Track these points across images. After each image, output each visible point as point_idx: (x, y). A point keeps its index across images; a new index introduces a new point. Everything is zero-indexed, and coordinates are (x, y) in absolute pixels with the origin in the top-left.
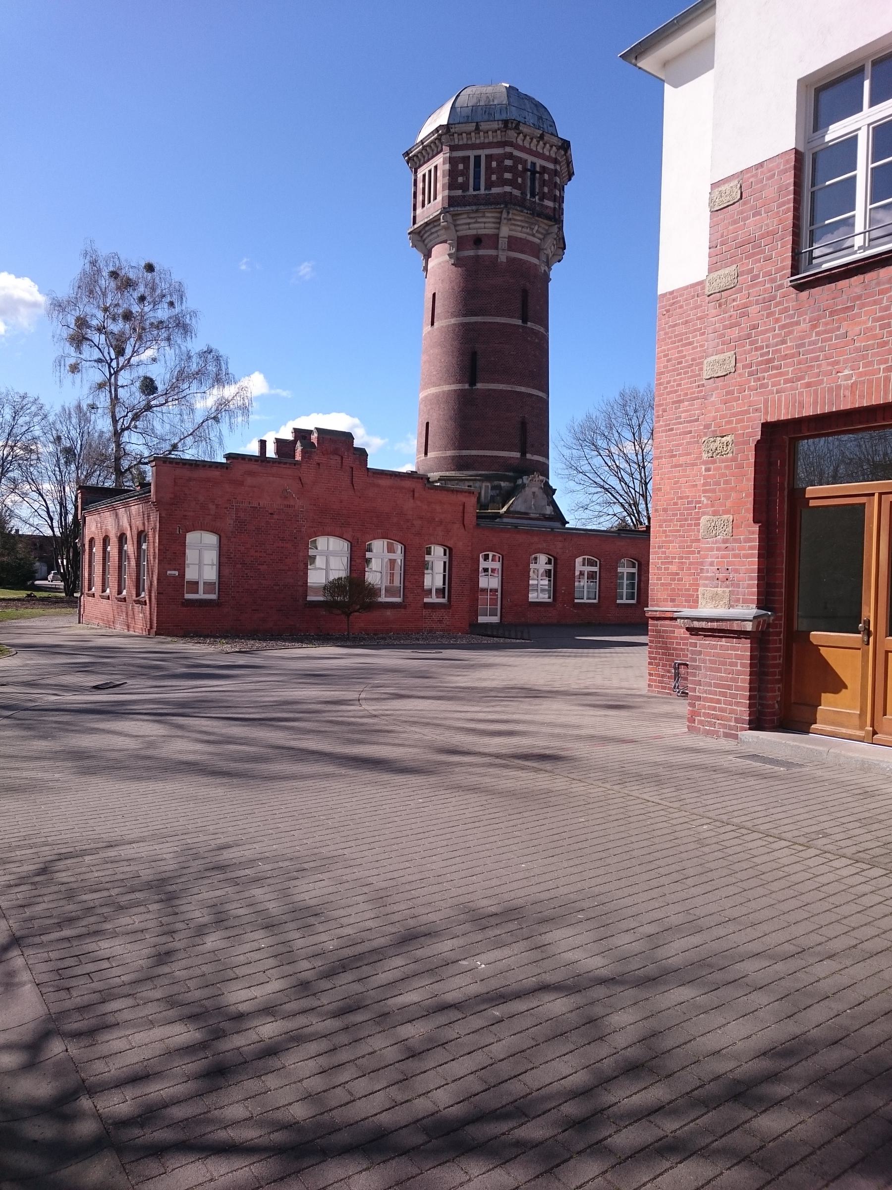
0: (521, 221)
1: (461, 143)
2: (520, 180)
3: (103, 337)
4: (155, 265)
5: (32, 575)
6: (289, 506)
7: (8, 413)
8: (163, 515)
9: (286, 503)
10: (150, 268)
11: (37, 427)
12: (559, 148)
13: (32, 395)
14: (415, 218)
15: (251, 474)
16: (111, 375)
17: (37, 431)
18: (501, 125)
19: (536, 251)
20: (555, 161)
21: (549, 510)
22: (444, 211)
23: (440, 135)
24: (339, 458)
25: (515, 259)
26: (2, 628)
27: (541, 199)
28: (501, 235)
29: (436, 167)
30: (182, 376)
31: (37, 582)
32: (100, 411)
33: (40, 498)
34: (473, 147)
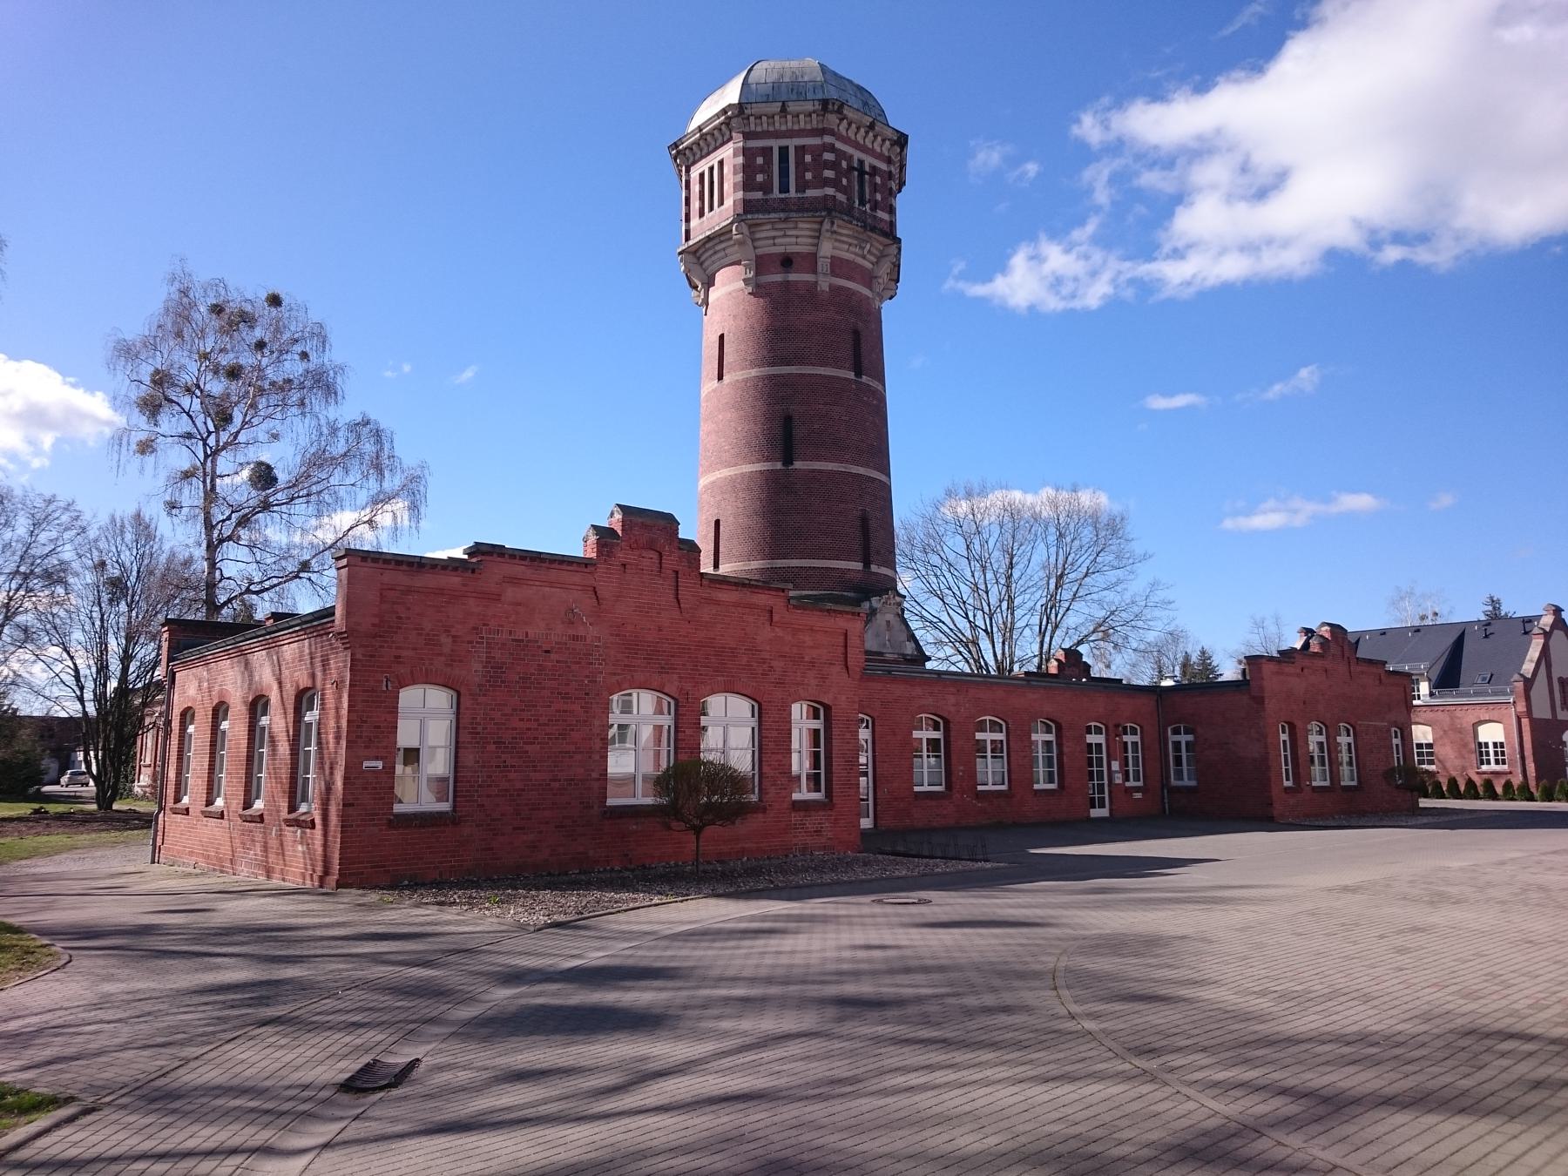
2: (844, 181)
3: (197, 401)
4: (283, 296)
5: (38, 778)
6: (575, 638)
7: (22, 526)
8: (359, 656)
9: (570, 632)
10: (275, 301)
11: (68, 547)
12: (894, 143)
13: (63, 497)
14: (688, 232)
15: (514, 581)
16: (206, 456)
17: (67, 554)
18: (818, 107)
19: (868, 279)
20: (889, 161)
21: (909, 649)
22: (738, 218)
23: (730, 118)
24: (655, 556)
25: (841, 288)
26: (6, 880)
27: (874, 208)
28: (821, 254)
29: (721, 163)
30: (319, 461)
31: (46, 789)
32: (185, 511)
33: (65, 655)
34: (777, 135)
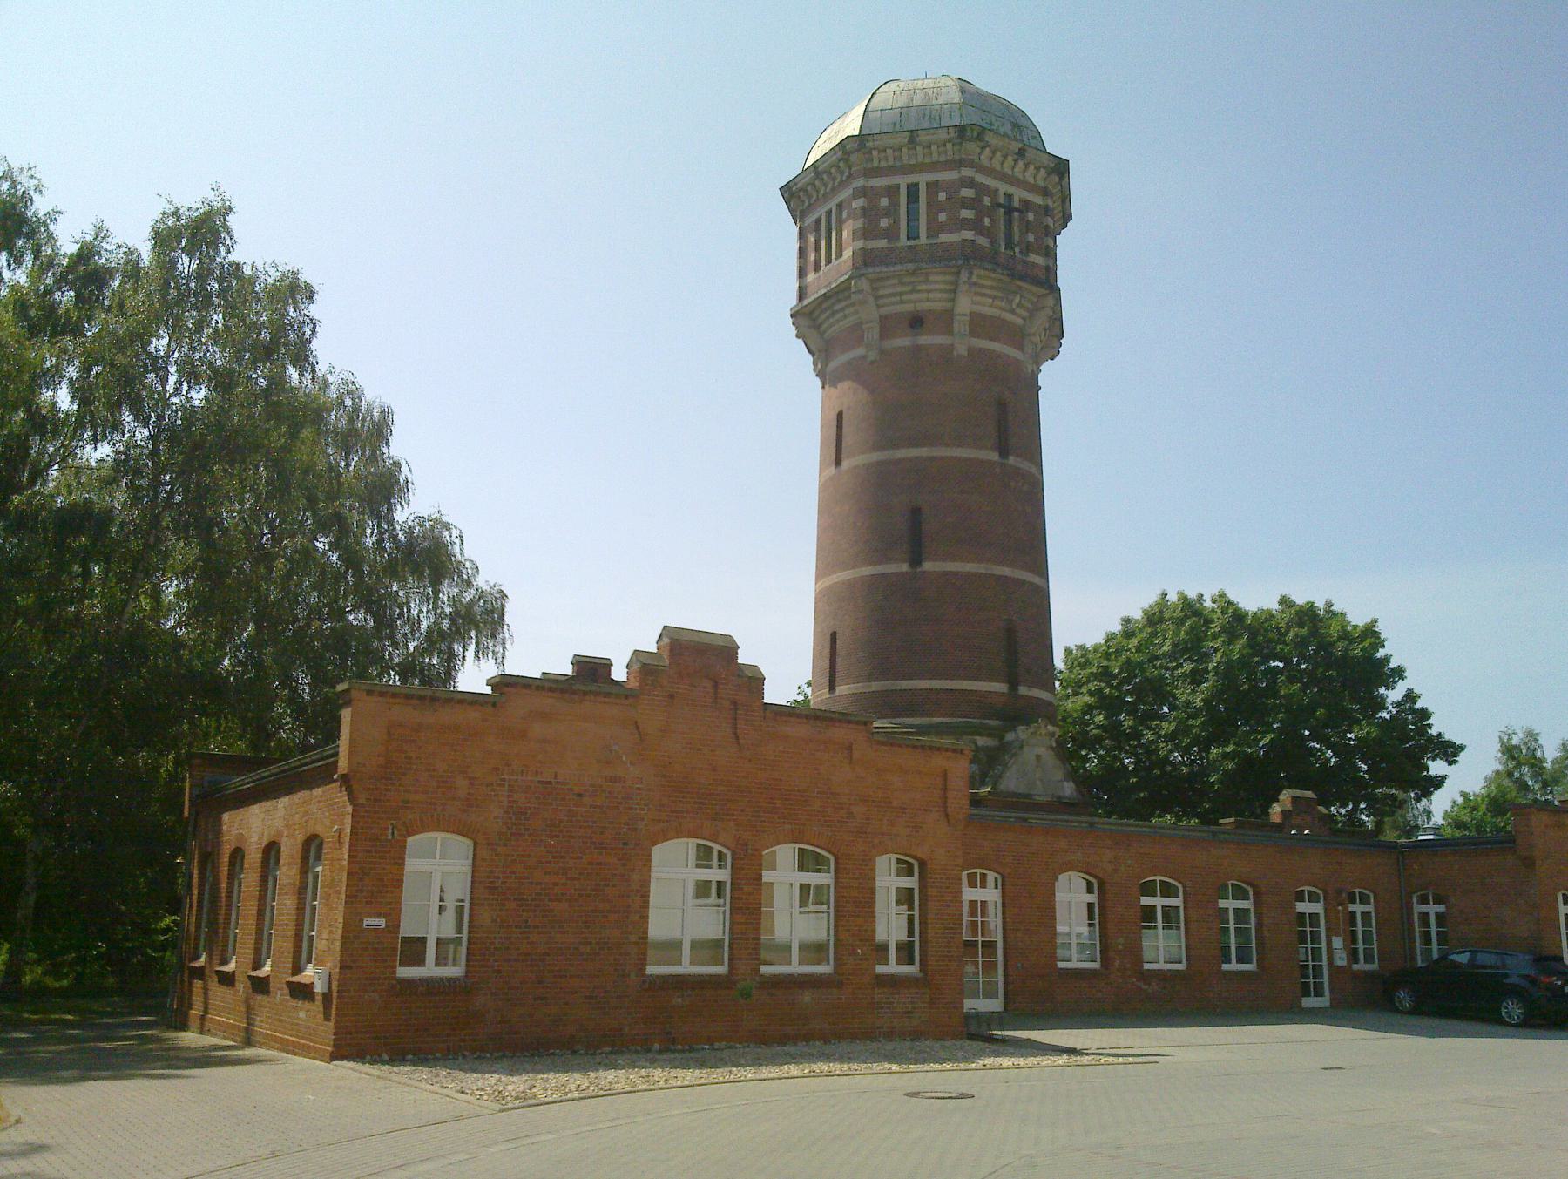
0: (991, 288)
1: (883, 164)
2: (987, 221)
6: (613, 780)
19: (1017, 337)
20: (1045, 192)
24: (709, 684)
